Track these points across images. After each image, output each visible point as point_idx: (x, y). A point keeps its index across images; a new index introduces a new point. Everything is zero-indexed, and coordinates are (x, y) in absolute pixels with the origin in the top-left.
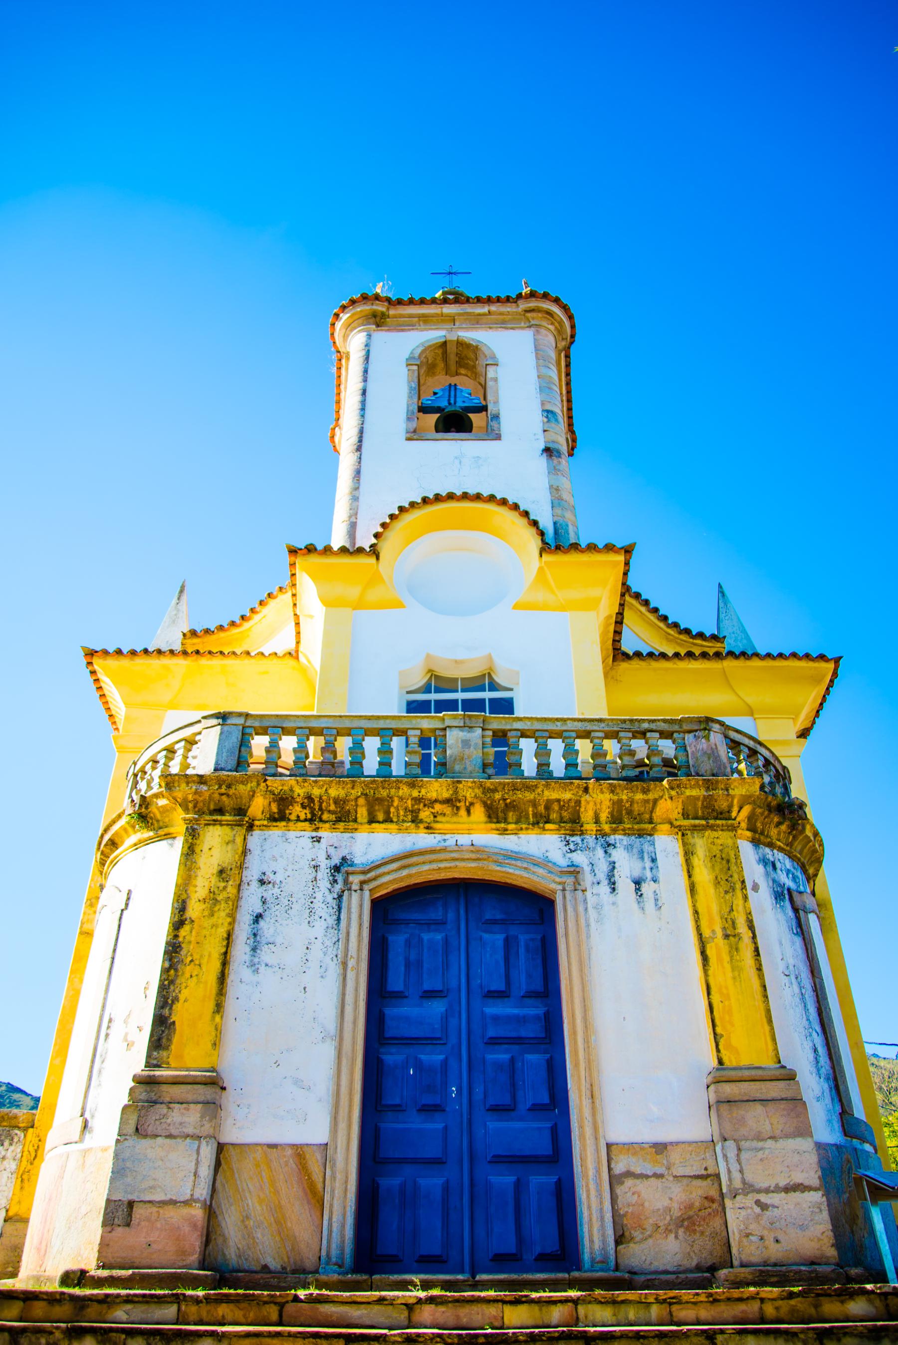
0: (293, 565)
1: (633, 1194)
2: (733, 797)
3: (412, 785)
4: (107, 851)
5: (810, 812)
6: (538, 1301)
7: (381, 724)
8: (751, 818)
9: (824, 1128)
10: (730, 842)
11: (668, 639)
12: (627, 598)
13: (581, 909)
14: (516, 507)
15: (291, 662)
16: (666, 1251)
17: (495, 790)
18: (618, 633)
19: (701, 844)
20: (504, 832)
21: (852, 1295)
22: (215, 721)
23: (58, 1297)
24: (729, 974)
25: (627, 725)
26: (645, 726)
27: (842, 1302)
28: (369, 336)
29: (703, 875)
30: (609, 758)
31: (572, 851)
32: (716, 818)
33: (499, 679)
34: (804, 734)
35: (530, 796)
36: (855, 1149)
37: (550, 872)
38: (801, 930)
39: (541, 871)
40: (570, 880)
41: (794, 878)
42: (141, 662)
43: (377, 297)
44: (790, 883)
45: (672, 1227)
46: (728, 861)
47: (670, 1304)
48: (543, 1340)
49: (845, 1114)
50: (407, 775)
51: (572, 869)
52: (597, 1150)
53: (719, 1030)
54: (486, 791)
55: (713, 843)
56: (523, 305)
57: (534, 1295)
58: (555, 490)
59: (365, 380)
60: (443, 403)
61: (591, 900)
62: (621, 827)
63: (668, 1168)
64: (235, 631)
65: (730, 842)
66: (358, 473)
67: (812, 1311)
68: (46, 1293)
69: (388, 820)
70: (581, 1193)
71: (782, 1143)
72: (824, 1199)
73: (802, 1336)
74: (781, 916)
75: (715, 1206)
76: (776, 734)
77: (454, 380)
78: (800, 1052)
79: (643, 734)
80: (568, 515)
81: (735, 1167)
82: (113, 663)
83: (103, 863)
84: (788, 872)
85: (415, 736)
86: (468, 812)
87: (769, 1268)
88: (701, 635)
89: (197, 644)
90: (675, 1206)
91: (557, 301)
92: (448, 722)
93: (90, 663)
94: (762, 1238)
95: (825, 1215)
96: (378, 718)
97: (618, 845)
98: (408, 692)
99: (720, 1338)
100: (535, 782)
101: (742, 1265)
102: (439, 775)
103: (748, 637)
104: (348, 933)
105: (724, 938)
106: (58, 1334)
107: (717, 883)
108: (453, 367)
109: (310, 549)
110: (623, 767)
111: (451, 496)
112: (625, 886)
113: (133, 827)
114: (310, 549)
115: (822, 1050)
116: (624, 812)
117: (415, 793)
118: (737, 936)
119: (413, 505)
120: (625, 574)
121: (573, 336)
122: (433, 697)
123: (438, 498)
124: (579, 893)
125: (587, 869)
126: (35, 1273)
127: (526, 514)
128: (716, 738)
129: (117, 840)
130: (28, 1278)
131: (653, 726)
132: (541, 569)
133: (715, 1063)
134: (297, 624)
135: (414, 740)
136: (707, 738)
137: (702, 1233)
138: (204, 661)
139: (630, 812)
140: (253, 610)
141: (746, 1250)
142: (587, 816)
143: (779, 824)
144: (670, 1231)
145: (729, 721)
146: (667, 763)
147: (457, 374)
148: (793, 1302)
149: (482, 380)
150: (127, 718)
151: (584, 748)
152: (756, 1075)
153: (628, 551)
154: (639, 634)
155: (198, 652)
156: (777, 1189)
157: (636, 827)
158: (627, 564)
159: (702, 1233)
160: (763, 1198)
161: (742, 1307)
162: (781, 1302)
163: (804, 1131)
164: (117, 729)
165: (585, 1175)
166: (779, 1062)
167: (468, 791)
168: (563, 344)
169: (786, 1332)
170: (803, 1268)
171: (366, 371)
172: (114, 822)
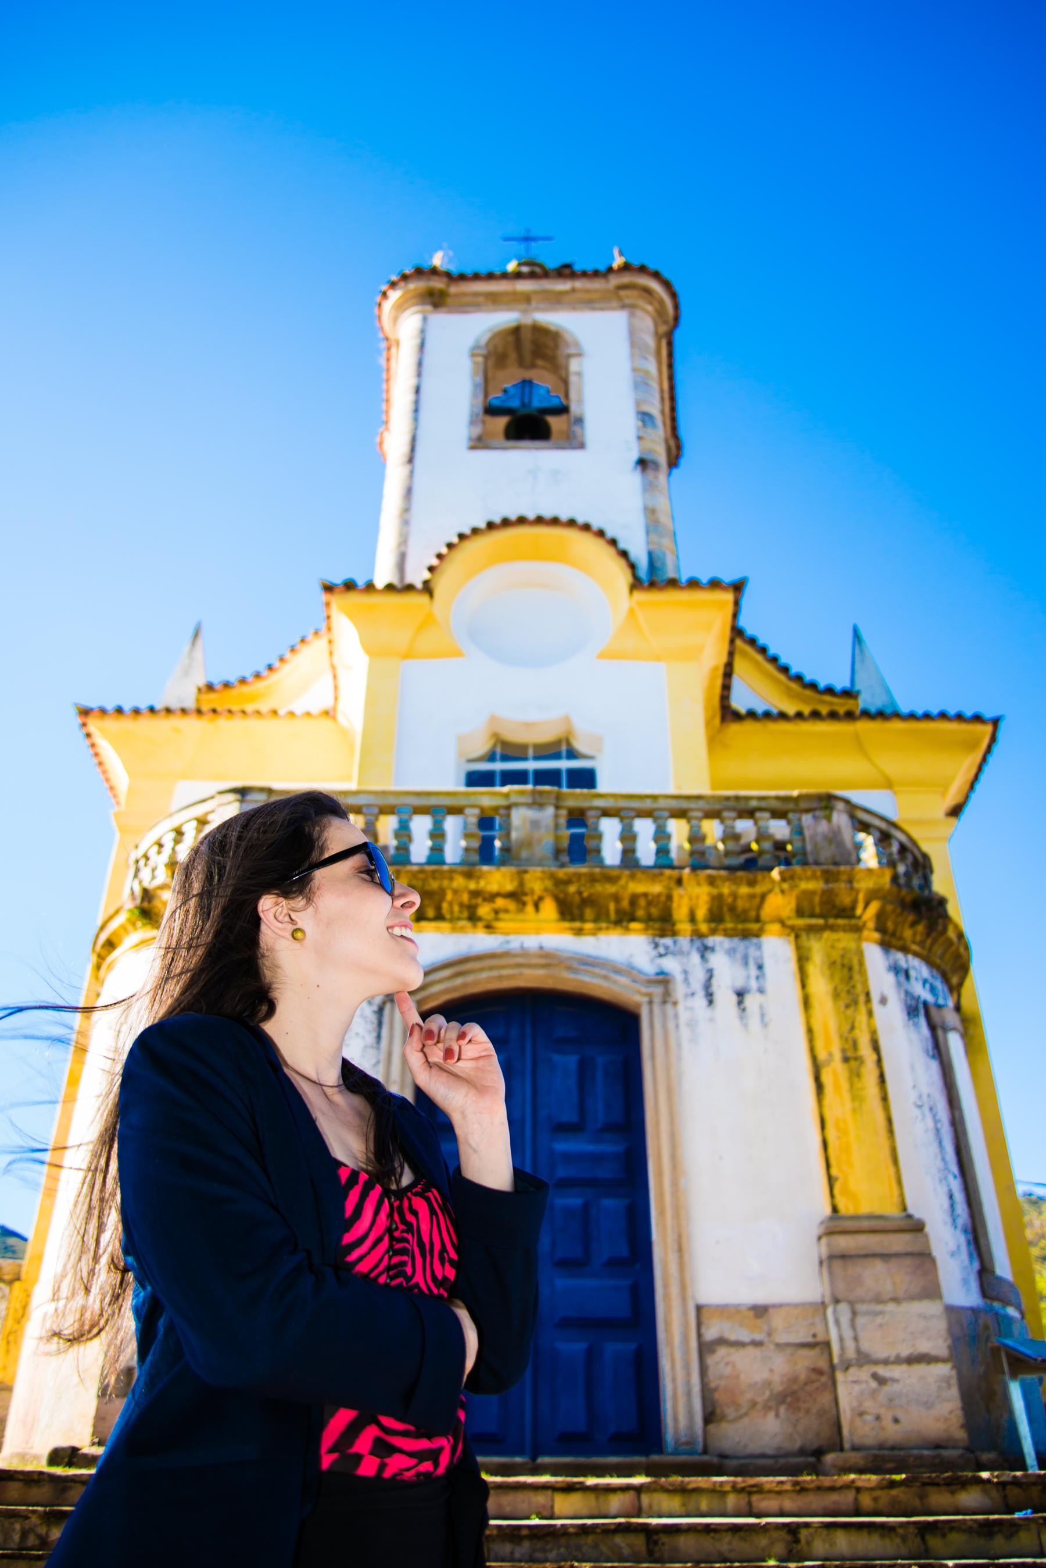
0: (328, 605)
1: (727, 1364)
2: (858, 892)
3: (469, 876)
4: (104, 953)
5: (951, 909)
6: (595, 1489)
7: (433, 801)
8: (880, 917)
9: (958, 1287)
10: (852, 945)
11: (790, 694)
12: (739, 643)
13: (671, 1025)
14: (601, 533)
15: (327, 723)
16: (768, 1431)
17: (568, 882)
18: (726, 687)
19: (817, 948)
20: (579, 932)
21: (964, 1484)
22: (232, 797)
23: (36, 1477)
24: (848, 1105)
25: (732, 804)
26: (754, 804)
27: (953, 1493)
28: (425, 320)
29: (820, 985)
30: (709, 842)
31: (661, 956)
32: (837, 916)
33: (579, 746)
34: (955, 811)
35: (611, 889)
36: (996, 1314)
37: (634, 981)
38: (939, 1052)
39: (623, 980)
40: (657, 991)
41: (933, 989)
42: (146, 725)
43: (434, 271)
44: (926, 995)
45: (772, 1404)
46: (850, 969)
47: (750, 1493)
48: (596, 1533)
49: (985, 1272)
50: (464, 863)
51: (661, 977)
52: (685, 1313)
53: (834, 1171)
54: (559, 883)
55: (833, 947)
56: (614, 281)
57: (591, 1481)
58: (650, 512)
59: (419, 374)
60: (515, 403)
61: (684, 1015)
62: (722, 927)
63: (769, 1334)
64: (260, 685)
65: (852, 945)
66: (409, 492)
67: (917, 1502)
68: (22, 1472)
69: (439, 917)
70: (665, 1364)
71: (905, 1307)
72: (954, 1372)
73: (901, 1531)
74: (914, 1036)
75: (824, 1379)
76: (918, 814)
77: (528, 374)
78: (931, 1198)
79: (751, 814)
80: (666, 542)
81: (848, 1334)
82: (112, 724)
83: (98, 967)
84: (925, 982)
85: (473, 815)
86: (537, 906)
87: (886, 1452)
88: (829, 690)
89: (216, 700)
90: (776, 1378)
91: (656, 275)
92: (514, 799)
93: (84, 725)
94: (878, 1418)
95: (954, 1392)
96: (429, 794)
97: (717, 948)
98: (470, 761)
99: (804, 1533)
100: (615, 873)
101: (855, 1448)
102: (503, 863)
103: (887, 691)
104: (390, 1054)
105: (846, 1061)
106: (34, 1519)
107: (836, 995)
108: (528, 357)
109: (350, 586)
110: (727, 853)
111: (522, 521)
112: (725, 997)
113: (134, 924)
114: (350, 586)
115: (959, 1197)
116: (725, 909)
117: (472, 885)
118: (859, 1059)
119: (475, 531)
120: (735, 616)
121: (676, 319)
122: (499, 766)
123: (506, 523)
124: (669, 1007)
125: (679, 977)
126: (20, 1450)
127: (613, 542)
128: (840, 818)
129: (115, 940)
130: (13, 1456)
131: (763, 804)
132: (631, 612)
133: (828, 1211)
134: (335, 677)
135: (473, 820)
136: (829, 818)
137: (808, 1411)
138: (222, 722)
139: (732, 909)
140: (282, 659)
141: (858, 1429)
142: (680, 912)
143: (913, 924)
144: (770, 1408)
145: (857, 797)
146: (780, 846)
147: (533, 366)
148: (894, 1492)
149: (563, 374)
150: (131, 791)
151: (678, 831)
152: (876, 1225)
153: (738, 587)
154: (752, 690)
155: (214, 711)
156: (898, 1361)
157: (740, 926)
158: (737, 603)
159: (808, 1411)
160: (882, 1371)
161: (834, 1497)
162: (878, 1493)
163: (932, 1291)
164: (118, 803)
165: (670, 1342)
166: (905, 1209)
167: (536, 882)
168: (663, 329)
169: (882, 1525)
170: (926, 1452)
171: (420, 364)
172: (110, 918)
